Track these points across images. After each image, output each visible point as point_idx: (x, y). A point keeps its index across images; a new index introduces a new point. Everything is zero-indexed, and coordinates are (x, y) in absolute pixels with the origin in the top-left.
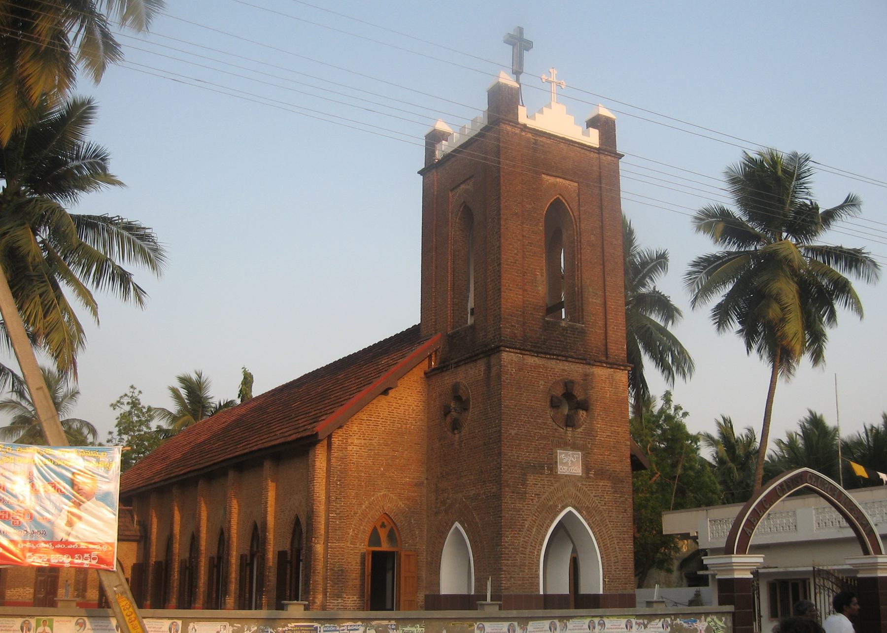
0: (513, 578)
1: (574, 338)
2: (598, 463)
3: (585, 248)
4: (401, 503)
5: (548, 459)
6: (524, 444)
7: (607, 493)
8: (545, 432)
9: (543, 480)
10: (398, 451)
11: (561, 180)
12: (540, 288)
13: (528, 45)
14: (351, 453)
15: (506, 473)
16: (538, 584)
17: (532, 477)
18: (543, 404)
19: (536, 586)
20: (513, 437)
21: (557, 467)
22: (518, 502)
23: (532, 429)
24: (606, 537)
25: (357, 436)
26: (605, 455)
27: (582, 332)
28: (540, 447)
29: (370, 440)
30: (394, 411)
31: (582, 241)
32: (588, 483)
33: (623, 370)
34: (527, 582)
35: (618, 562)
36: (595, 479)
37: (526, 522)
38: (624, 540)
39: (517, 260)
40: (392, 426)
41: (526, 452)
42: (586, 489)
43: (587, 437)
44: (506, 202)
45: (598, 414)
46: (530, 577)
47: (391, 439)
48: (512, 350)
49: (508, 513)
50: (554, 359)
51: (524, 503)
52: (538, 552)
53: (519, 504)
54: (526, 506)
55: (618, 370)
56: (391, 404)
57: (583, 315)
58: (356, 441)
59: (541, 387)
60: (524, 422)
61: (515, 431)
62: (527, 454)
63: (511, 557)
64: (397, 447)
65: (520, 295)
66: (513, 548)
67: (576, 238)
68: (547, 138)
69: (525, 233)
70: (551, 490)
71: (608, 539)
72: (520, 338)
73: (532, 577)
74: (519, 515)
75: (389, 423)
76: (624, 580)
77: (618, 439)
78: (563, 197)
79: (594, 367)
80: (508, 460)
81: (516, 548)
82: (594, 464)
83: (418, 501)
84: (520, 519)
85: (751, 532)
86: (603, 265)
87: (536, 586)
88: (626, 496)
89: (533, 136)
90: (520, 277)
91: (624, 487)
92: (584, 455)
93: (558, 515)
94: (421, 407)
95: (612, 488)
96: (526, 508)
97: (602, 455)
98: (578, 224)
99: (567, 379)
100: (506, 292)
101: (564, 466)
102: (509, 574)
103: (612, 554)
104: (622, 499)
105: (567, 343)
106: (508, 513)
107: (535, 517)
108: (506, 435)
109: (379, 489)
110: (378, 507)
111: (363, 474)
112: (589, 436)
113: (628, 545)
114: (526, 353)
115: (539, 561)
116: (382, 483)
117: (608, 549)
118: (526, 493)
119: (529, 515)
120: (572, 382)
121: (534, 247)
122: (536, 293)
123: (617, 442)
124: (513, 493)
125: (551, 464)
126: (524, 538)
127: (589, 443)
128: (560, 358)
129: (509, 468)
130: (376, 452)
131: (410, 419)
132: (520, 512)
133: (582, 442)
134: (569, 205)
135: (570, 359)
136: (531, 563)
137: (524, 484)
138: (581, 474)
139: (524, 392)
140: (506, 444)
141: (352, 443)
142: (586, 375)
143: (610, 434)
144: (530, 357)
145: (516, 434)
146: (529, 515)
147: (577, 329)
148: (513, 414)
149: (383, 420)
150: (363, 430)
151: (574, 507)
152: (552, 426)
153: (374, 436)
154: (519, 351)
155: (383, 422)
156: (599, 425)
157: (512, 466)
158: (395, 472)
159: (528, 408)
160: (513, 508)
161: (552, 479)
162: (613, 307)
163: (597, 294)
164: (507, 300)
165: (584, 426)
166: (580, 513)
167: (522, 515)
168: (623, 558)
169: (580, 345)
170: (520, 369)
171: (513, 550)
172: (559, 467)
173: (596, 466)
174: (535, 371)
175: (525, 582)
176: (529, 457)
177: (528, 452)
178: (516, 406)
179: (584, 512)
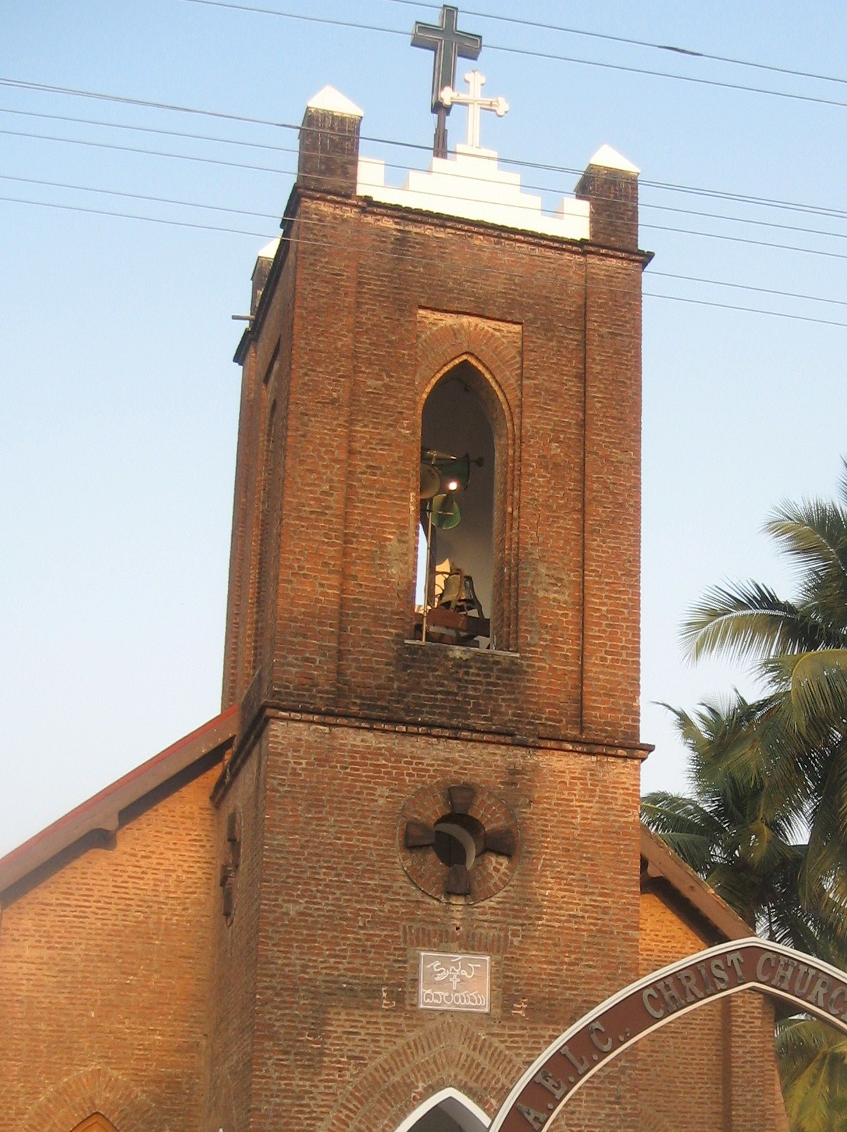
1: (489, 684)
2: (542, 984)
3: (531, 475)
4: (138, 1090)
5: (390, 972)
6: (324, 936)
9: (376, 1023)
10: (135, 975)
12: (394, 571)
13: (470, 47)
14: (15, 977)
15: (268, 1007)
17: (343, 1017)
18: (384, 841)
21: (415, 992)
23: (348, 901)
25: (31, 941)
26: (563, 963)
27: (513, 671)
29: (63, 948)
30: (129, 885)
31: (525, 456)
32: (507, 1032)
33: (625, 757)
39: (328, 507)
40: (120, 917)
41: (330, 956)
42: (502, 1046)
43: (510, 920)
44: (306, 374)
45: (543, 865)
47: (119, 947)
48: (298, 716)
49: (269, 1103)
50: (418, 734)
54: (322, 1085)
55: (611, 760)
56: (120, 868)
57: (517, 632)
58: (28, 953)
59: (381, 801)
60: (326, 886)
61: (301, 908)
64: (133, 963)
65: (331, 587)
67: (511, 452)
68: (435, 225)
69: (356, 446)
70: (395, 1047)
72: (327, 688)
79: (540, 752)
80: (273, 976)
82: (526, 984)
83: (184, 1087)
85: (542, 1117)
86: (583, 511)
89: (396, 223)
90: (333, 544)
92: (498, 963)
93: (414, 1108)
94: (199, 874)
96: (322, 1089)
97: (551, 963)
98: (516, 421)
99: (457, 781)
100: (290, 582)
101: (440, 989)
105: (466, 696)
106: (269, 1103)
108: (271, 916)
109: (84, 1060)
112: (515, 917)
114: (339, 721)
116: (91, 1047)
119: (331, 1107)
120: (470, 790)
121: (384, 475)
122: (383, 581)
123: (599, 931)
127: (515, 934)
128: (435, 731)
129: (278, 995)
130: (79, 975)
131: (170, 902)
132: (303, 1098)
133: (493, 932)
134: (494, 377)
135: (465, 734)
138: (487, 1010)
139: (328, 813)
140: (271, 938)
141: (17, 957)
142: (514, 772)
143: (580, 914)
144: (351, 731)
146: (331, 1107)
147: (497, 663)
148: (295, 866)
151: (464, 1088)
153: (74, 941)
154: (316, 717)
156: (549, 889)
157: (287, 990)
159: (340, 851)
161: (401, 1020)
162: (604, 608)
163: (561, 580)
164: (293, 599)
165: (501, 894)
167: (307, 1106)
170: (322, 761)
172: (423, 991)
174: (366, 765)
177: (335, 956)
178: (302, 847)
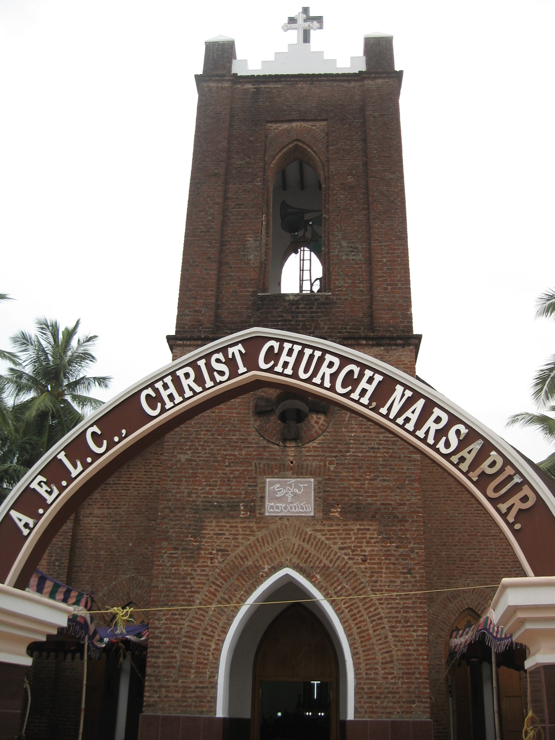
0: (165, 687)
5: (246, 493)
7: (367, 542)
8: (244, 453)
9: (236, 527)
11: (299, 124)
16: (214, 698)
17: (214, 524)
19: (209, 702)
20: (183, 464)
21: (263, 505)
22: (183, 563)
23: (218, 450)
24: (366, 617)
26: (365, 479)
28: (232, 476)
30: (153, 470)
32: (327, 528)
34: (193, 695)
35: (392, 662)
36: (343, 520)
37: (197, 595)
38: (407, 622)
40: (148, 489)
41: (206, 485)
43: (327, 454)
46: (197, 687)
49: (163, 582)
51: (195, 565)
52: (217, 644)
53: (185, 566)
58: (96, 512)
60: (205, 442)
62: (208, 488)
63: (163, 653)
66: (168, 638)
71: (369, 621)
73: (202, 688)
74: (184, 583)
75: (144, 486)
76: (405, 695)
77: (394, 453)
78: (302, 142)
80: (170, 500)
81: (174, 638)
82: (340, 495)
84: (185, 591)
87: (209, 702)
88: (411, 545)
91: (407, 530)
92: (319, 482)
95: (380, 533)
96: (199, 572)
97: (357, 480)
101: (279, 502)
102: (157, 681)
103: (377, 648)
104: (401, 550)
105: (297, 321)
106: (163, 582)
107: (214, 587)
110: (121, 595)
111: (102, 552)
112: (331, 452)
113: (415, 631)
115: (217, 659)
117: (369, 639)
118: (200, 549)
119: (204, 584)
124: (176, 549)
125: (253, 501)
126: (191, 621)
127: (331, 463)
129: (172, 512)
130: (124, 522)
132: (186, 578)
136: (201, 663)
137: (198, 532)
138: (312, 514)
140: (169, 477)
141: (91, 514)
145: (188, 460)
146: (204, 584)
149: (136, 482)
150: (108, 497)
151: (297, 568)
152: (256, 443)
155: (135, 484)
158: (150, 548)
160: (174, 574)
162: (384, 260)
166: (309, 577)
168: (403, 655)
169: (321, 321)
171: (168, 642)
172: (268, 504)
173: (346, 498)
175: (188, 695)
176: (211, 494)
179: (318, 576)
